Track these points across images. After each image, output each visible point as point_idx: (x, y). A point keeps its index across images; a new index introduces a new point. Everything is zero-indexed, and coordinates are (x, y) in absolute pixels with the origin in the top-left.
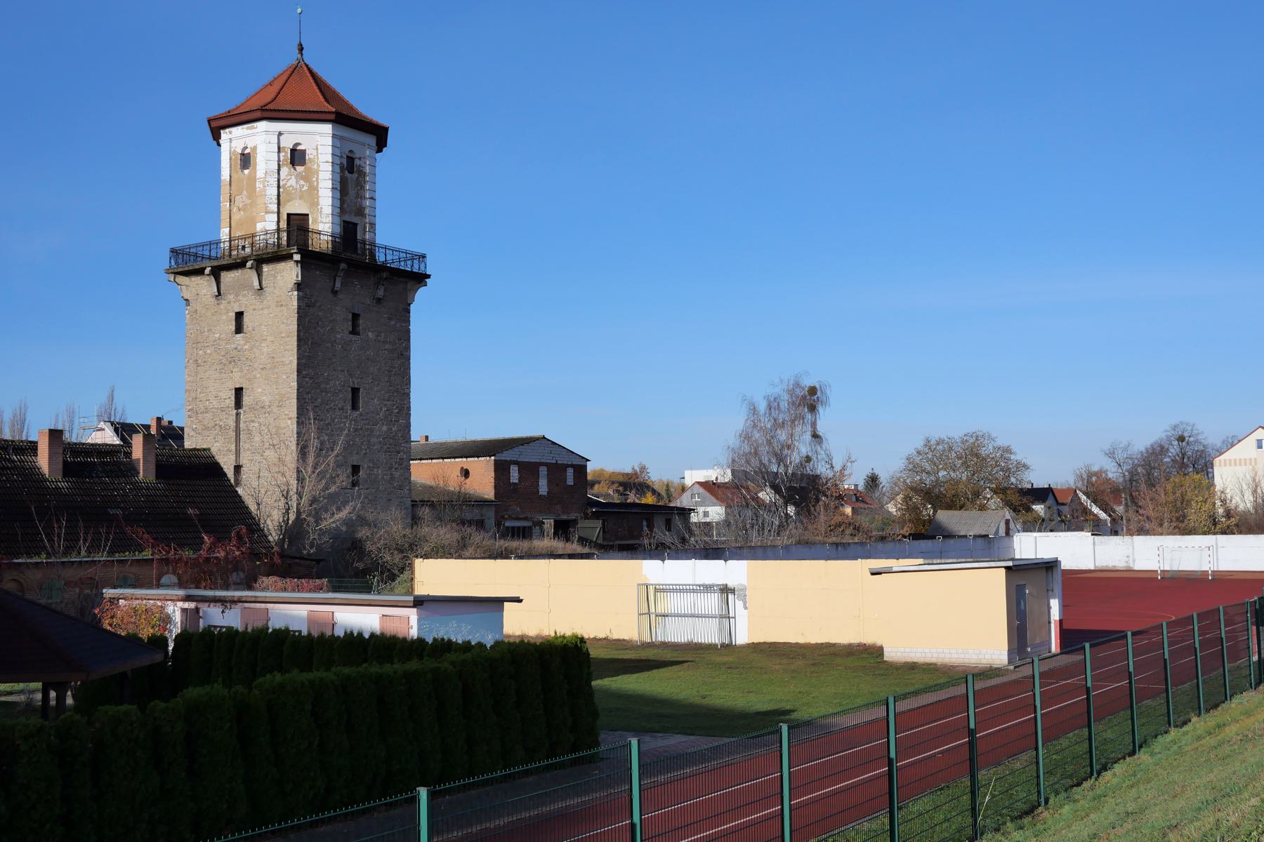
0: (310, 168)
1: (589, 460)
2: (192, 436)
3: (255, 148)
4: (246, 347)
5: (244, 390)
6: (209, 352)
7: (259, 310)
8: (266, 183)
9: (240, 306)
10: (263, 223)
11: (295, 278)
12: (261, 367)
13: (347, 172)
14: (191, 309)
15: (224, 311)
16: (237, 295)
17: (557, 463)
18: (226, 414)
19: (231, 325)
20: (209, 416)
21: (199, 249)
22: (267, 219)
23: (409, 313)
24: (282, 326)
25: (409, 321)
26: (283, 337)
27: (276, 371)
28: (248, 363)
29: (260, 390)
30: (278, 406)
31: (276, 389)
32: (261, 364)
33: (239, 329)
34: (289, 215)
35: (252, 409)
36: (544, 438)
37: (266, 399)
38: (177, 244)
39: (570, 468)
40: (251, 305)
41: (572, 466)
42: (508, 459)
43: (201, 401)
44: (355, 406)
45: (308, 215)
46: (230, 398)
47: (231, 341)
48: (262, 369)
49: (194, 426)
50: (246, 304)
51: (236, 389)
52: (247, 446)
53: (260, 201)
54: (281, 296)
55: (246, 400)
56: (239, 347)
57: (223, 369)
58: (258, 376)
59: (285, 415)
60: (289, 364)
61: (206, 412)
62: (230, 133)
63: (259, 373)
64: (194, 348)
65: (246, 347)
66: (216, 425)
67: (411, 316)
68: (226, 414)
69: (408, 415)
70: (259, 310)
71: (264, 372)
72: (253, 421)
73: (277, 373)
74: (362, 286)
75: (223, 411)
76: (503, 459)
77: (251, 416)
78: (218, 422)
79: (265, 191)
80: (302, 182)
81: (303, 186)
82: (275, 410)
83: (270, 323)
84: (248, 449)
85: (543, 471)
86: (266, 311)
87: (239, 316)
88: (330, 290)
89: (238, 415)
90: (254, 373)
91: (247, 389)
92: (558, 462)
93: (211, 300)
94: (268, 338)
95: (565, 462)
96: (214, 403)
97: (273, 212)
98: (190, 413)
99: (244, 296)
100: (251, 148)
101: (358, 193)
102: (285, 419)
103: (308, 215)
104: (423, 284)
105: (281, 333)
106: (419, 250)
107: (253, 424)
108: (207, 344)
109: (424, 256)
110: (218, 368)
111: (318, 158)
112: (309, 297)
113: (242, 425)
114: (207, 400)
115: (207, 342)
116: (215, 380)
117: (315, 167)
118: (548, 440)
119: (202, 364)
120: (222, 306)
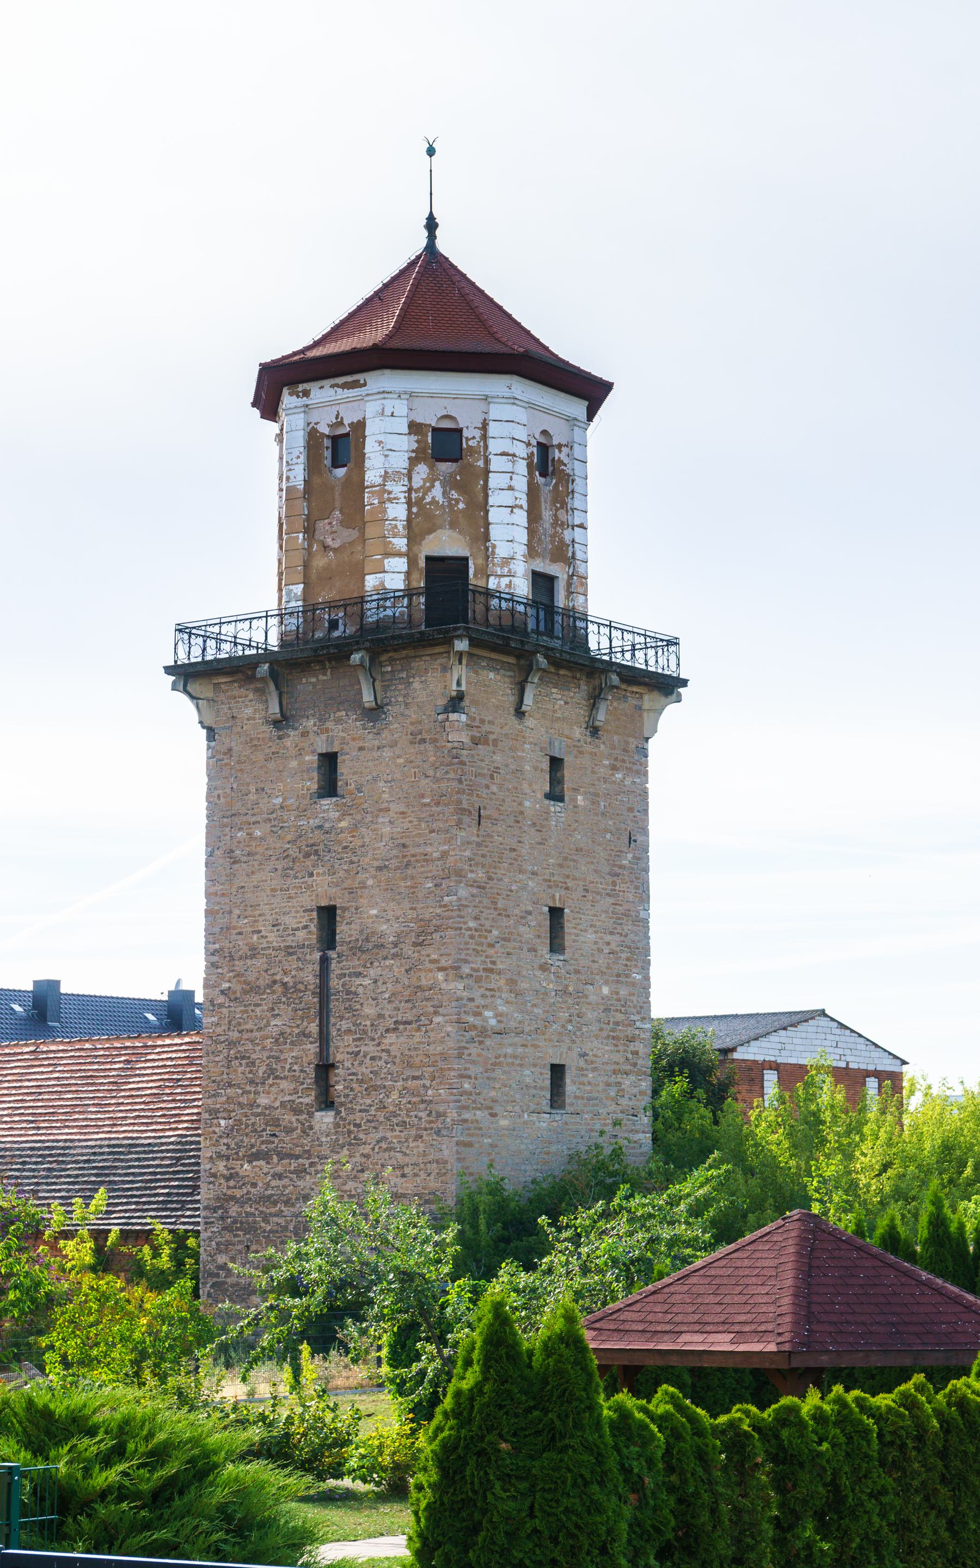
0: (471, 466)
1: (907, 1063)
2: (221, 1006)
3: (360, 426)
4: (343, 824)
5: (338, 912)
6: (258, 833)
7: (372, 749)
8: (386, 496)
9: (330, 741)
10: (378, 575)
11: (454, 687)
12: (376, 864)
13: (537, 473)
14: (218, 748)
15: (293, 752)
16: (322, 720)
17: (847, 1068)
18: (299, 959)
19: (311, 779)
20: (260, 963)
21: (240, 625)
22: (387, 568)
23: (646, 756)
24: (424, 782)
25: (646, 774)
26: (425, 805)
27: (410, 871)
28: (347, 856)
29: (374, 912)
30: (415, 944)
31: (411, 909)
32: (377, 859)
33: (329, 787)
34: (429, 559)
35: (357, 949)
36: (823, 1013)
37: (388, 930)
38: (189, 617)
39: (873, 1079)
40: (354, 739)
41: (877, 1074)
42: (760, 1058)
43: (240, 933)
44: (556, 944)
45: (466, 559)
46: (306, 927)
47: (308, 813)
48: (380, 869)
49: (227, 985)
50: (344, 738)
51: (321, 909)
52: (345, 1025)
53: (371, 531)
54: (420, 722)
55: (345, 931)
56: (327, 825)
57: (292, 869)
58: (370, 882)
59: (431, 962)
60: (439, 859)
61: (253, 956)
62: (306, 394)
63: (375, 877)
64: (225, 826)
65: (343, 824)
66: (275, 982)
67: (650, 764)
68: (299, 959)
69: (645, 966)
70: (372, 749)
71: (384, 875)
72: (358, 975)
73: (412, 878)
74: (566, 703)
75: (291, 954)
76: (751, 1057)
77: (354, 963)
78: (278, 977)
79: (384, 511)
80: (454, 495)
81: (457, 501)
82: (408, 950)
83: (398, 776)
84: (349, 1031)
85: (771, 1078)
86: (387, 753)
87: (329, 761)
88: (512, 710)
89: (325, 961)
90: (361, 876)
91: (344, 909)
92: (851, 1066)
93: (265, 728)
94: (392, 806)
95: (863, 1067)
96: (272, 937)
97: (399, 555)
98: (215, 959)
99: (339, 721)
100: (351, 425)
101: (555, 515)
102: (431, 971)
103: (466, 559)
104: (674, 697)
105: (423, 796)
106: (666, 630)
107: (358, 981)
108: (254, 819)
109: (672, 642)
110: (280, 867)
111: (486, 447)
112: (477, 724)
113: (335, 983)
114: (254, 932)
115: (254, 815)
116: (273, 890)
117: (481, 463)
118: (833, 1020)
119: (244, 859)
120: (288, 742)
